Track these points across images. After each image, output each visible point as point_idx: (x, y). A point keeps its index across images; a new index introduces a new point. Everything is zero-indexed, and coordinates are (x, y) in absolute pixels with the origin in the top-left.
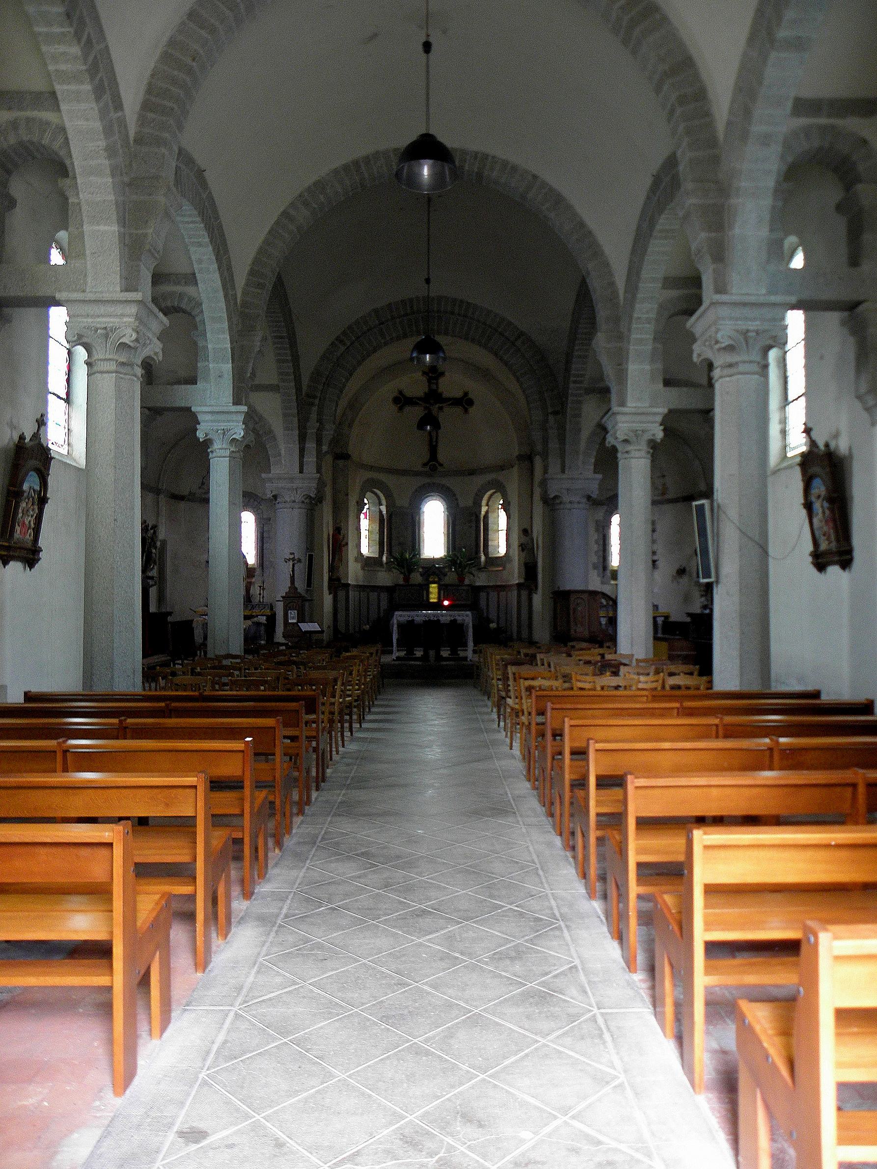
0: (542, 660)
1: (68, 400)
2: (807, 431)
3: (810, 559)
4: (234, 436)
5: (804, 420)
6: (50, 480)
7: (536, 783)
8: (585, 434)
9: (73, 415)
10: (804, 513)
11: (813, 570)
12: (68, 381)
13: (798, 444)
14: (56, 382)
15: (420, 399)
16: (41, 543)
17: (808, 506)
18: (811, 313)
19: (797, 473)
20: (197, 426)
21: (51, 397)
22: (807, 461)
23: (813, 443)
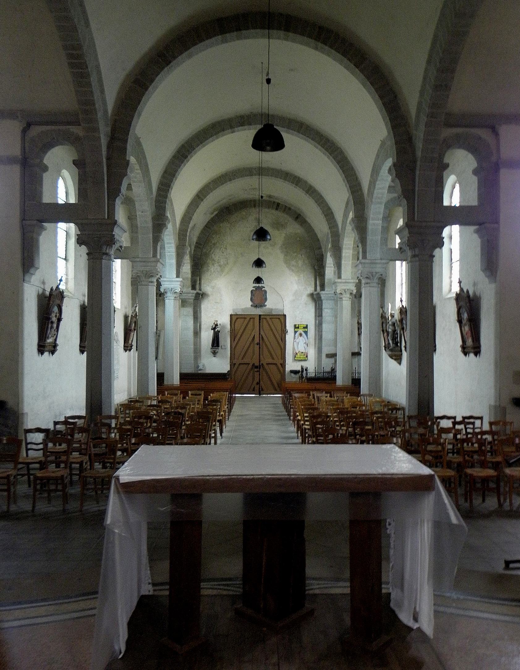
0: (313, 395)
1: (66, 259)
2: (460, 282)
3: (460, 349)
4: (151, 275)
5: (459, 277)
6: (64, 308)
7: (109, 348)
8: (390, 335)
9: (68, 265)
10: (458, 324)
11: (462, 355)
12: (66, 248)
13: (456, 289)
14: (61, 252)
15: (415, 416)
16: (58, 342)
17: (460, 321)
18: (463, 227)
19: (454, 303)
20: (80, 233)
21: (59, 259)
22: (459, 297)
23: (461, 289)
